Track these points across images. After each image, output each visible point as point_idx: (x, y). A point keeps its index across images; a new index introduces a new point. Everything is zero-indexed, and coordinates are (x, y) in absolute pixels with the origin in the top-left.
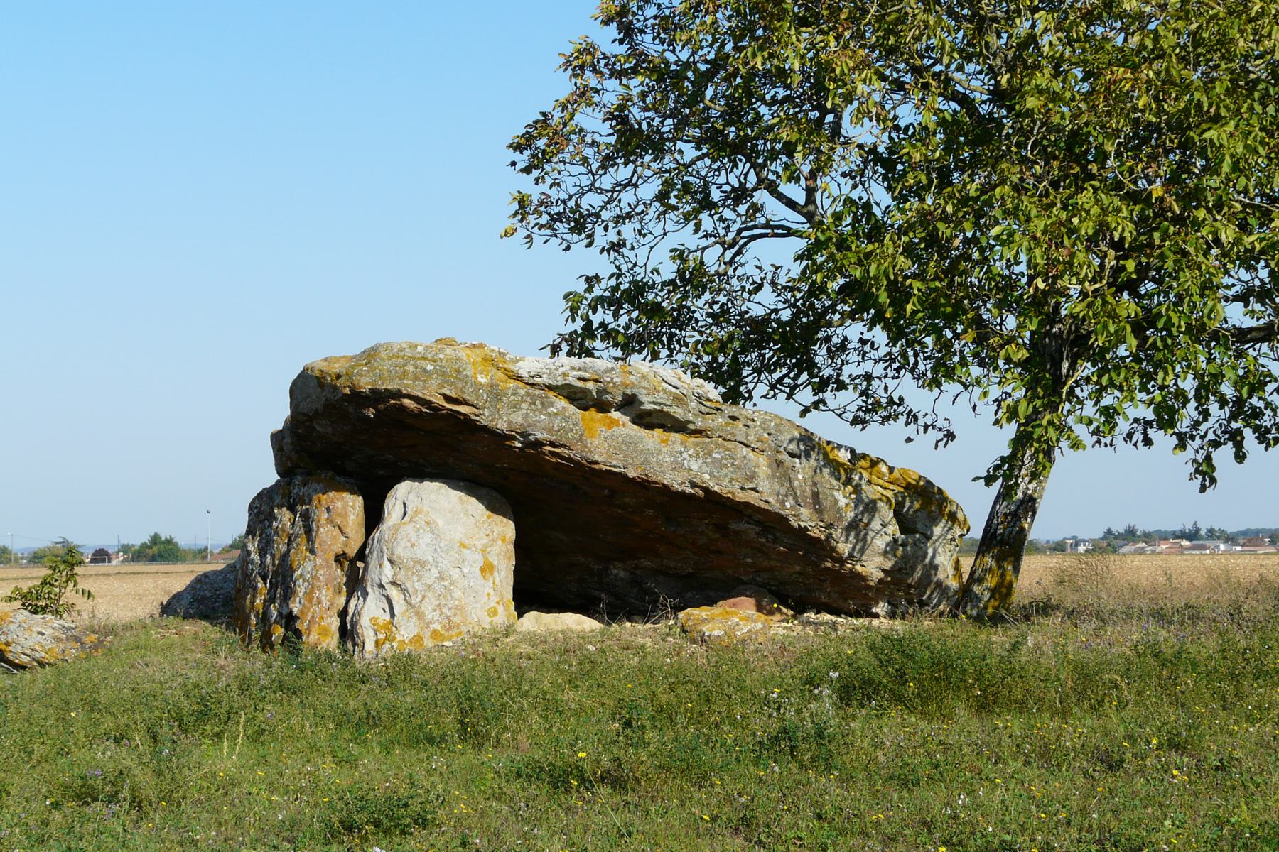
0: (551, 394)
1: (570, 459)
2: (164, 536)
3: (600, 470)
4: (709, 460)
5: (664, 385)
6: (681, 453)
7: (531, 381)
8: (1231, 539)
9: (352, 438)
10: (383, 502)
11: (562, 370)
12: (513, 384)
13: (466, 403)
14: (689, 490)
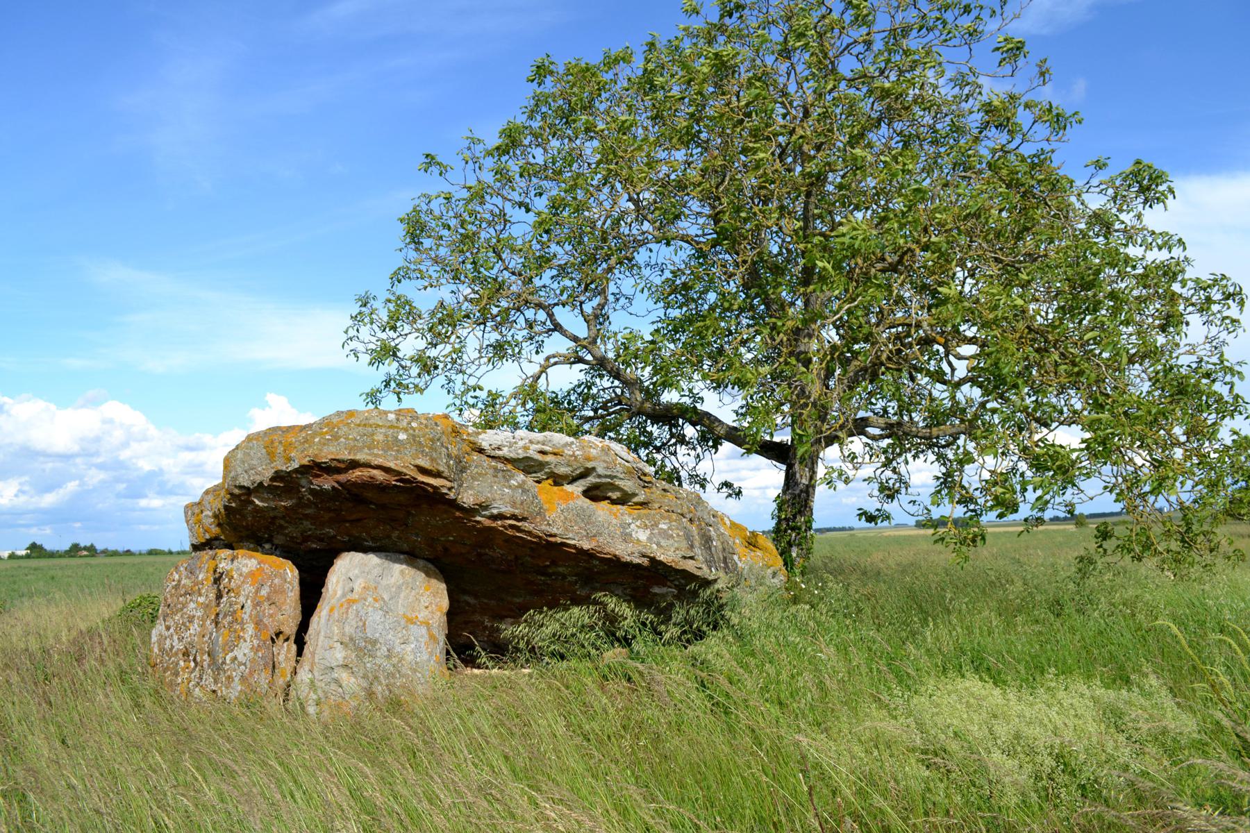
0: (509, 467)
1: (529, 533)
2: (38, 543)
3: (556, 544)
4: (656, 531)
10: (326, 576)
11: (521, 443)
12: (475, 456)
13: (438, 475)
14: (637, 561)
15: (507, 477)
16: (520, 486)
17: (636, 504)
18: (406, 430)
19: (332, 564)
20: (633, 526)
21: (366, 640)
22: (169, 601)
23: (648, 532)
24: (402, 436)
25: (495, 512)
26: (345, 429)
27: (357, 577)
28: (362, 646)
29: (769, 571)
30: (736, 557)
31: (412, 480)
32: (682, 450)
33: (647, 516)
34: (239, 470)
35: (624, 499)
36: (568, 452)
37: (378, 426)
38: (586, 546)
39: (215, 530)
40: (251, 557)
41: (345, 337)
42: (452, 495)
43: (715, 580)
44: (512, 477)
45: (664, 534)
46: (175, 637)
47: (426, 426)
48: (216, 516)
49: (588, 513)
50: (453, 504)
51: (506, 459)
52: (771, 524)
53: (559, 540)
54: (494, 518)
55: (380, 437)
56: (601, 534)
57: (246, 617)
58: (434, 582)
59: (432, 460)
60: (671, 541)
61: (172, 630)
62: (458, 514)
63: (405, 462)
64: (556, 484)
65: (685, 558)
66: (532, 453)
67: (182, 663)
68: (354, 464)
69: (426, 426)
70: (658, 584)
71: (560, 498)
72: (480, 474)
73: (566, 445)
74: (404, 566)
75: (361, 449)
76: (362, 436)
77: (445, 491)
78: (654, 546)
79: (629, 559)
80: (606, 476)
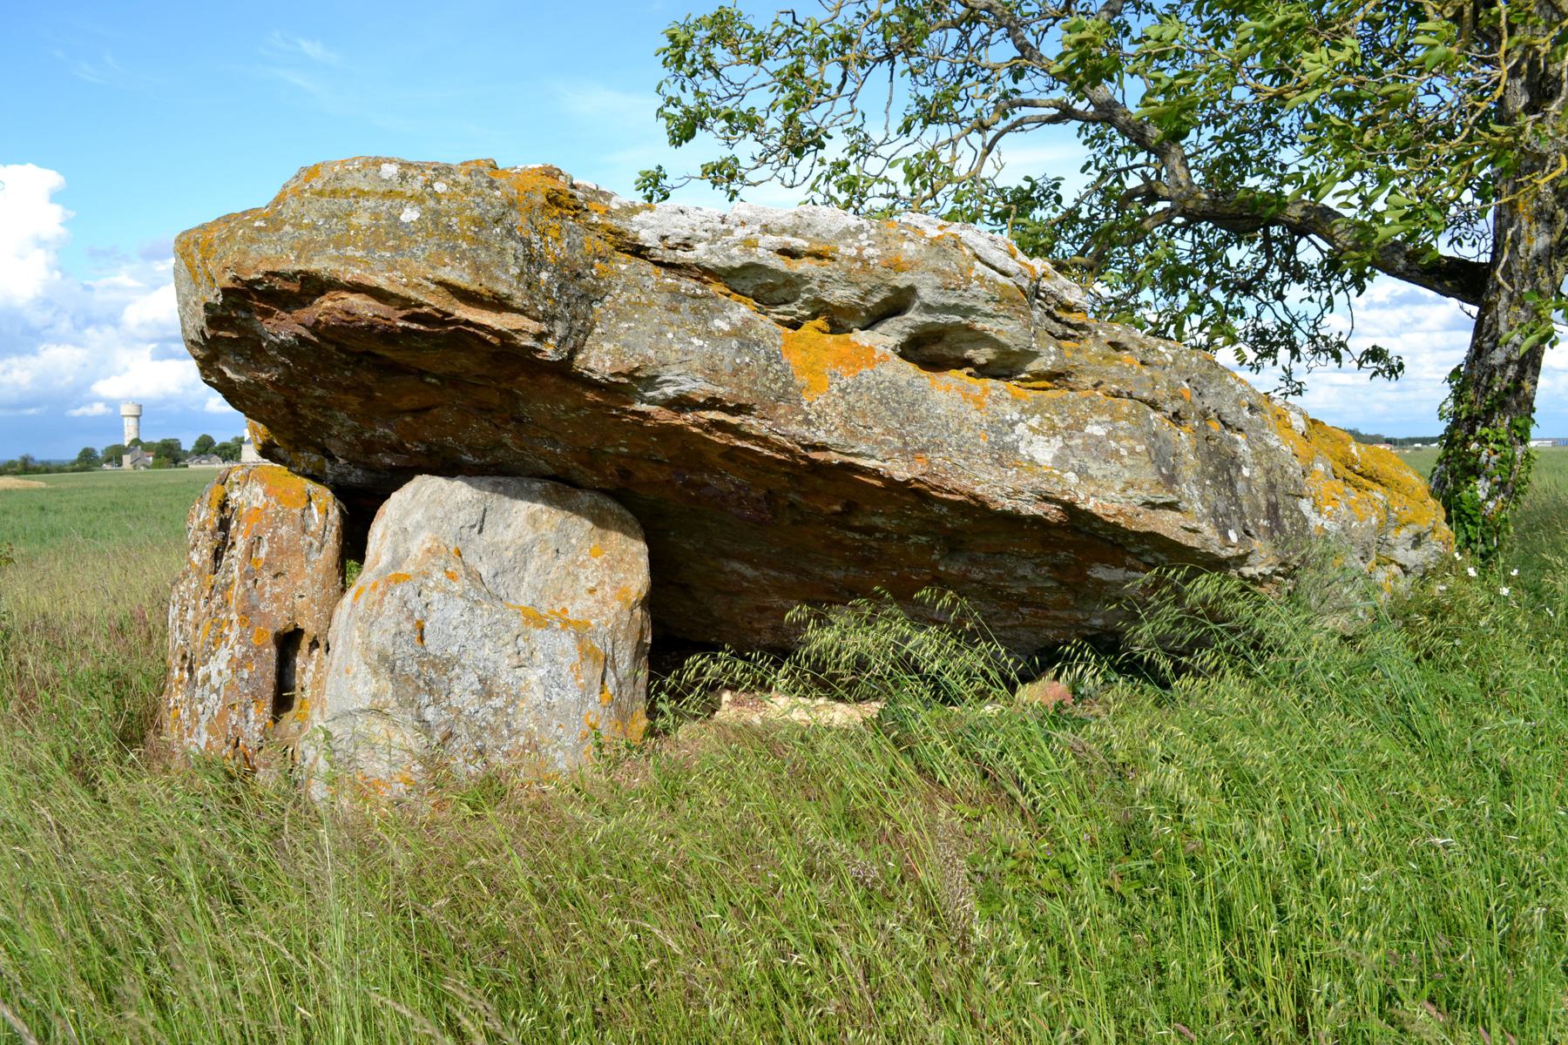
0: (715, 288)
1: (764, 440)
3: (828, 466)
4: (1077, 441)
5: (978, 264)
6: (1013, 424)
7: (669, 257)
8: (1389, 441)
9: (362, 382)
10: (366, 535)
11: (740, 233)
12: (623, 264)
13: (499, 304)
14: (1030, 509)
15: (703, 310)
16: (736, 333)
17: (1038, 376)
18: (418, 200)
20: (1020, 428)
21: (425, 659)
23: (1057, 442)
25: (670, 391)
27: (419, 527)
28: (417, 674)
29: (1406, 533)
30: (1305, 506)
31: (444, 319)
32: (1294, 292)
33: (1057, 405)
35: (1005, 366)
36: (847, 250)
37: (361, 193)
38: (901, 471)
42: (549, 352)
43: (1242, 560)
44: (719, 311)
45: (1097, 447)
47: (467, 190)
49: (908, 396)
50: (564, 371)
51: (706, 271)
52: (1439, 428)
53: (835, 458)
55: (363, 219)
56: (939, 447)
58: (615, 537)
59: (477, 268)
60: (1115, 467)
62: (590, 396)
63: (418, 273)
64: (836, 328)
65: (1153, 506)
66: (764, 255)
69: (467, 190)
70: (1102, 561)
71: (840, 361)
72: (636, 305)
73: (846, 233)
74: (539, 506)
76: (327, 219)
77: (528, 342)
78: (1072, 477)
79: (1009, 505)
80: (946, 309)
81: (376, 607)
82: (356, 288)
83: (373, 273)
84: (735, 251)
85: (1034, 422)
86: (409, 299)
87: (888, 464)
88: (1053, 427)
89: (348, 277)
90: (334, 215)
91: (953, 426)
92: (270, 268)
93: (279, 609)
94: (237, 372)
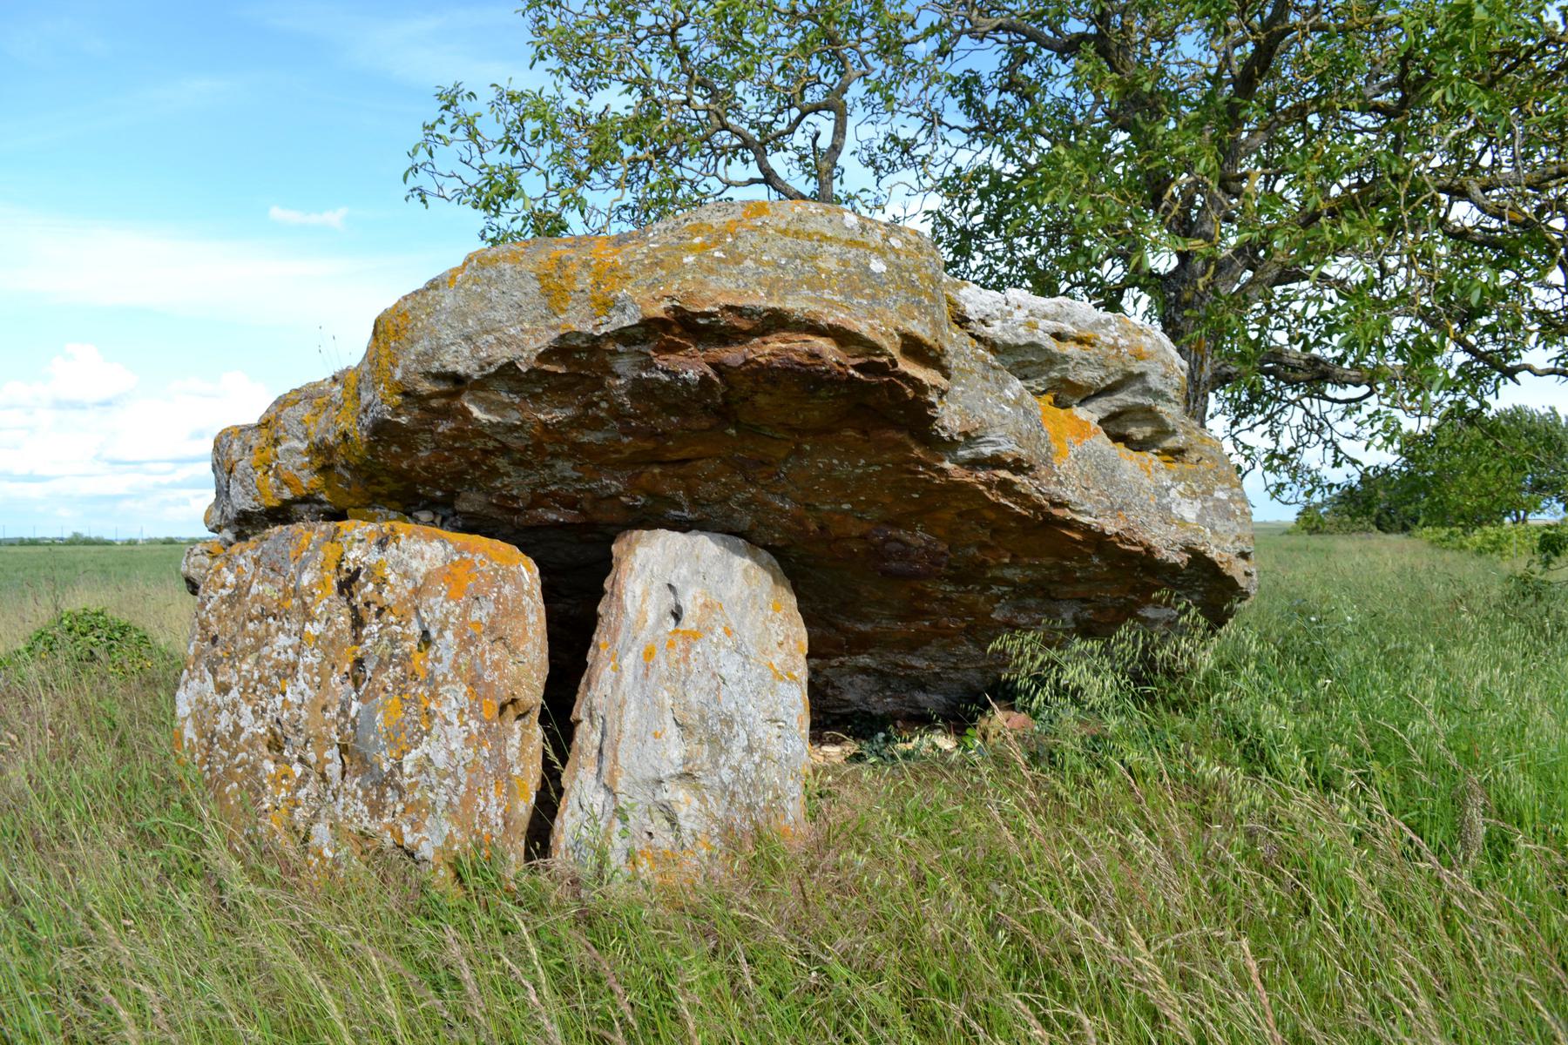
1: (1024, 498)
17: (1166, 452)
18: (882, 253)
19: (1098, 540)
20: (1173, 492)
22: (215, 629)
23: (1198, 504)
24: (877, 266)
25: (987, 451)
26: (756, 239)
34: (447, 335)
37: (824, 238)
39: (308, 480)
40: (430, 539)
41: (409, 163)
46: (246, 710)
48: (320, 450)
54: (976, 463)
57: (441, 669)
60: (1232, 524)
61: (234, 693)
67: (269, 766)
68: (777, 321)
73: (1098, 324)
75: (793, 288)
81: (682, 666)
82: (812, 328)
83: (857, 319)
84: (1021, 330)
85: (1180, 488)
86: (877, 347)
87: (1100, 520)
88: (1194, 492)
89: (831, 320)
90: (797, 256)
91: (1135, 490)
92: (731, 302)
93: (501, 678)
94: (488, 411)
